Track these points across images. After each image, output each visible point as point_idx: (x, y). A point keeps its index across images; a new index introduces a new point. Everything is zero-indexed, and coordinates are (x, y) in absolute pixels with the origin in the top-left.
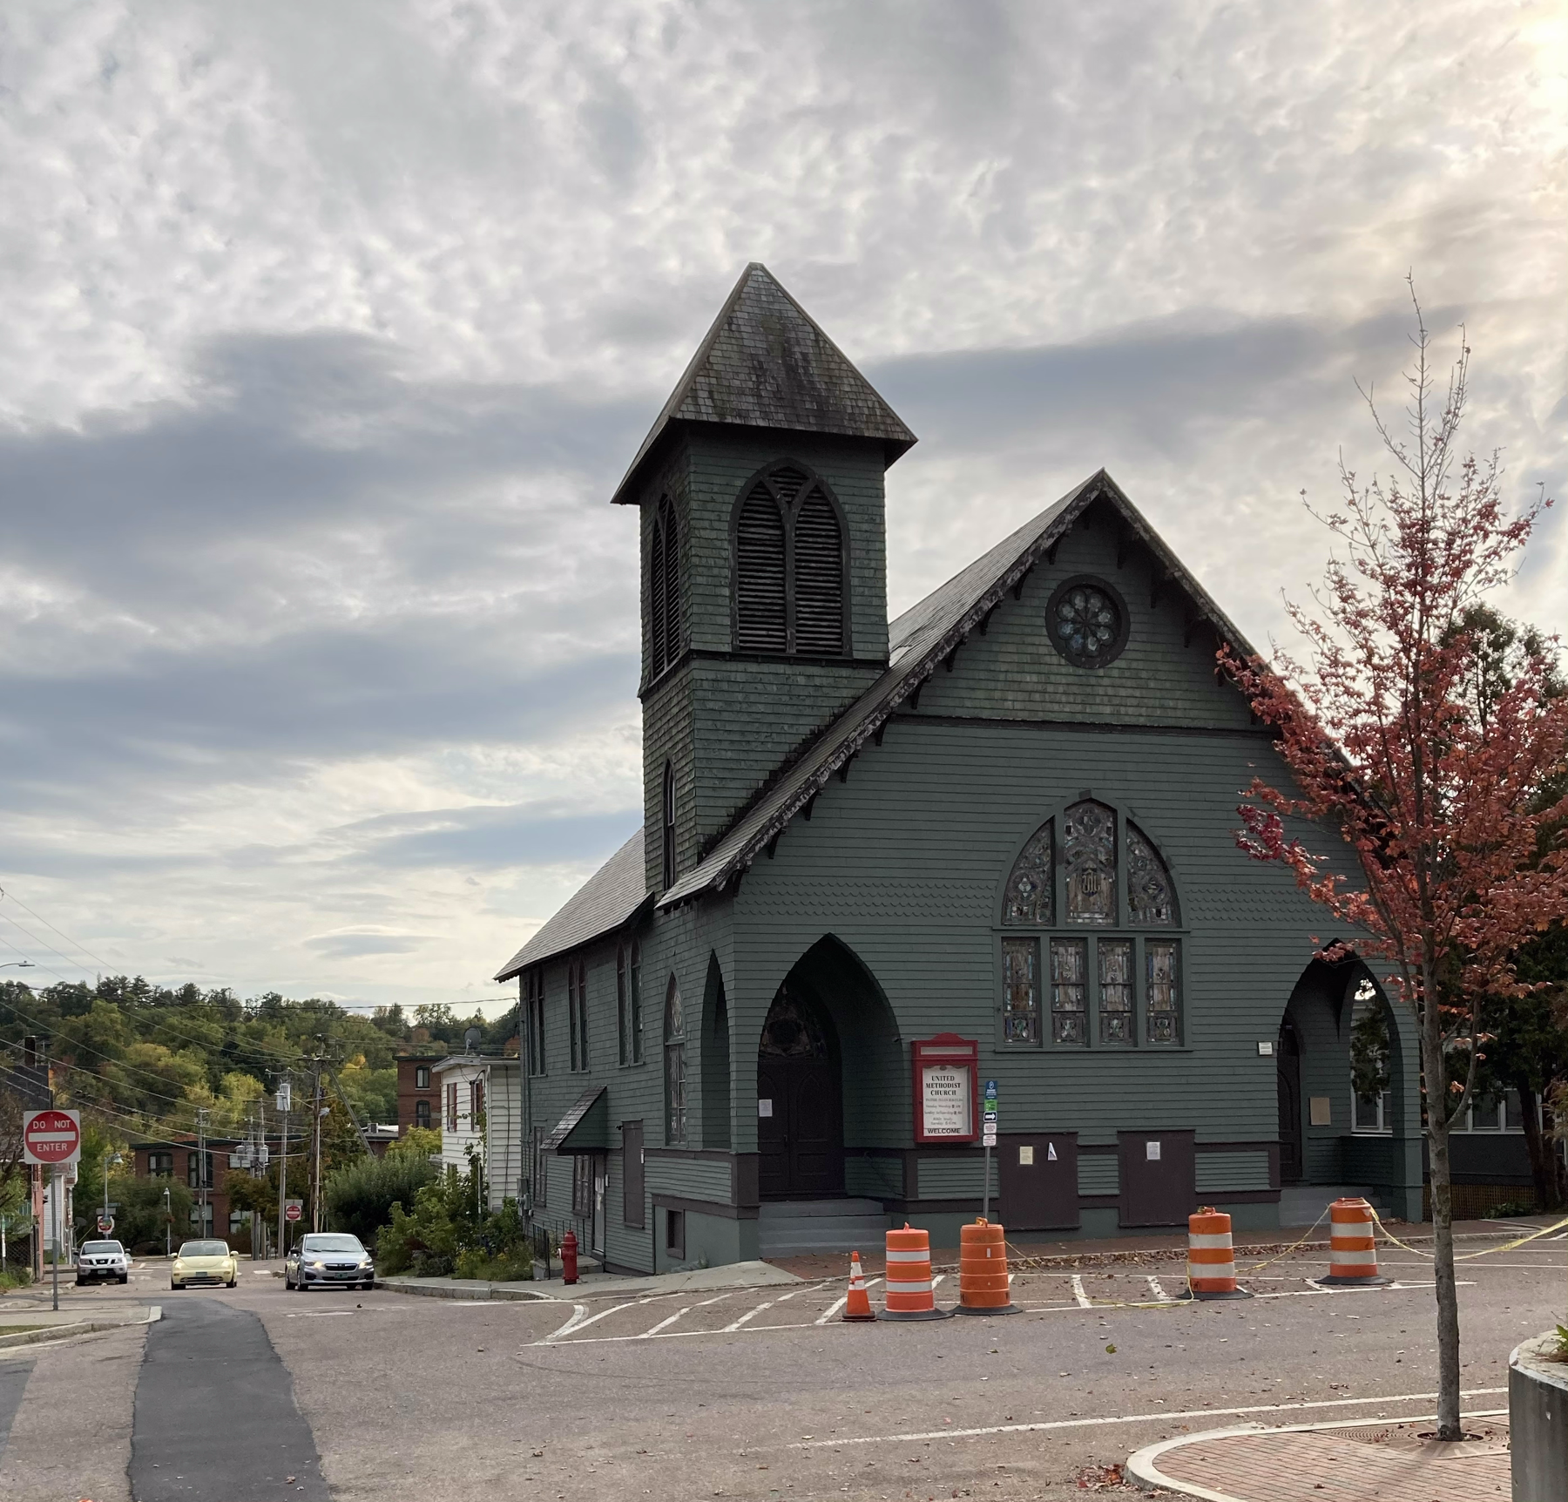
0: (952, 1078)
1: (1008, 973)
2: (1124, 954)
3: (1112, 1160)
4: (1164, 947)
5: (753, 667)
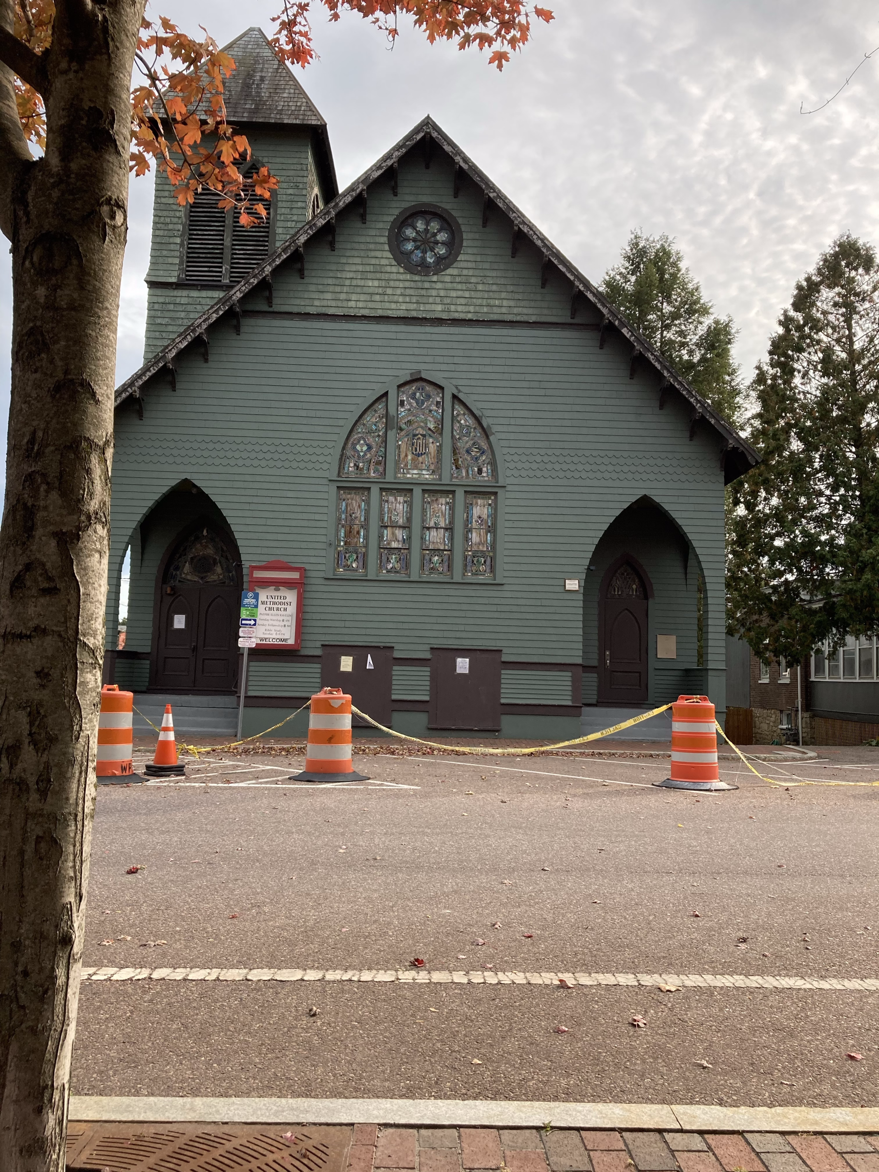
0: (285, 598)
1: (343, 516)
2: (447, 503)
3: (425, 672)
4: (483, 498)
5: (195, 294)
